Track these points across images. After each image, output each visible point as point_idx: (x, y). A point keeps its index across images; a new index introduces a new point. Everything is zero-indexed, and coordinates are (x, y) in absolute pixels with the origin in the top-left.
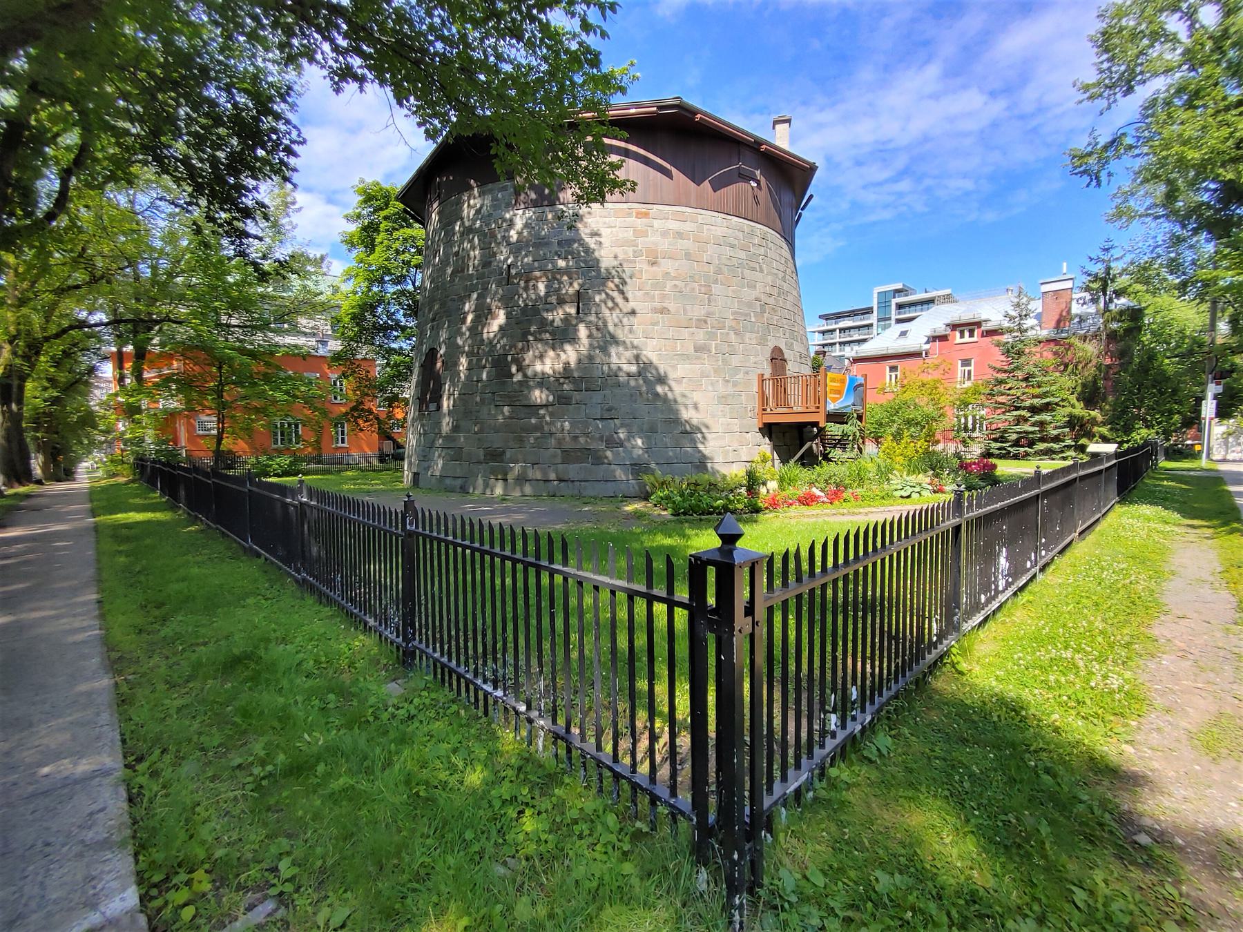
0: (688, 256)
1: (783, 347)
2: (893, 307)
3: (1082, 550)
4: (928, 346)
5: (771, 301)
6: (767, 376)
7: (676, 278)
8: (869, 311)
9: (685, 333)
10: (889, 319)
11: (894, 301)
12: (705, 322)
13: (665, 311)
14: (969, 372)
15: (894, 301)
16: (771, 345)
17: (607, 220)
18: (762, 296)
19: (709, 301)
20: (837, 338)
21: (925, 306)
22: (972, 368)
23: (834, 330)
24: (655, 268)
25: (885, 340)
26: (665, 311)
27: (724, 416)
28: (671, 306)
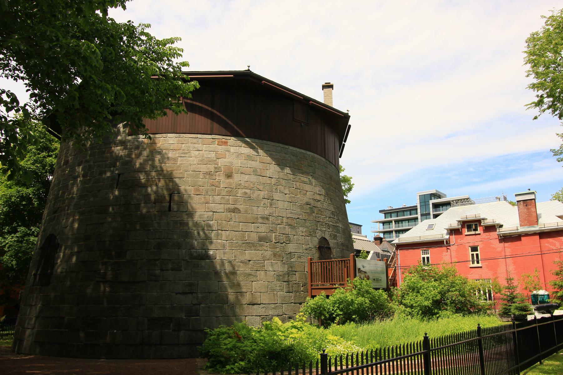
0: (255, 172)
1: (327, 237)
2: (431, 206)
3: (365, 326)
4: (447, 237)
5: (319, 205)
6: (316, 259)
7: (246, 188)
8: (414, 209)
9: (252, 227)
10: (429, 214)
11: (431, 202)
12: (267, 219)
13: (235, 210)
14: (477, 255)
15: (431, 202)
16: (319, 235)
17: (196, 145)
18: (312, 202)
19: (271, 205)
20: (393, 227)
21: (444, 208)
22: (478, 252)
23: (391, 222)
24: (230, 180)
25: (419, 232)
26: (235, 210)
27: (282, 290)
28: (241, 207)
